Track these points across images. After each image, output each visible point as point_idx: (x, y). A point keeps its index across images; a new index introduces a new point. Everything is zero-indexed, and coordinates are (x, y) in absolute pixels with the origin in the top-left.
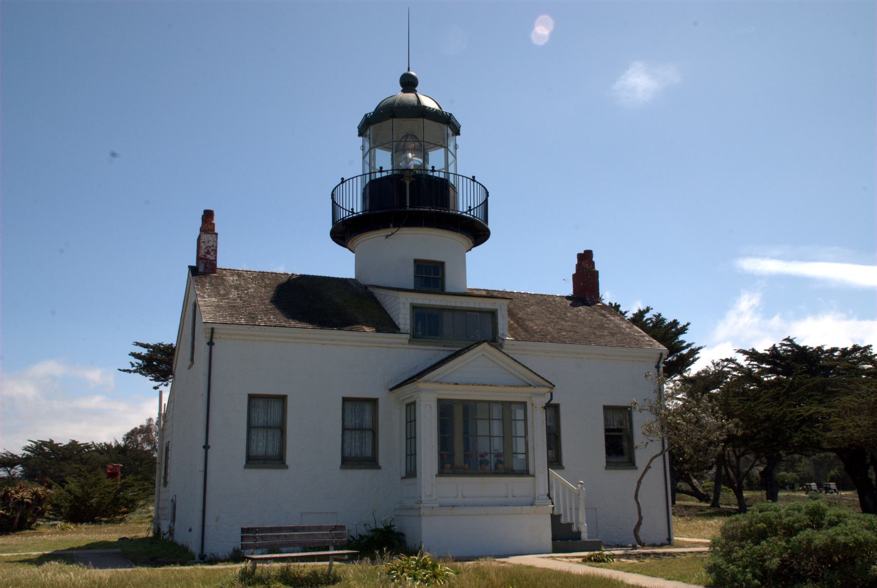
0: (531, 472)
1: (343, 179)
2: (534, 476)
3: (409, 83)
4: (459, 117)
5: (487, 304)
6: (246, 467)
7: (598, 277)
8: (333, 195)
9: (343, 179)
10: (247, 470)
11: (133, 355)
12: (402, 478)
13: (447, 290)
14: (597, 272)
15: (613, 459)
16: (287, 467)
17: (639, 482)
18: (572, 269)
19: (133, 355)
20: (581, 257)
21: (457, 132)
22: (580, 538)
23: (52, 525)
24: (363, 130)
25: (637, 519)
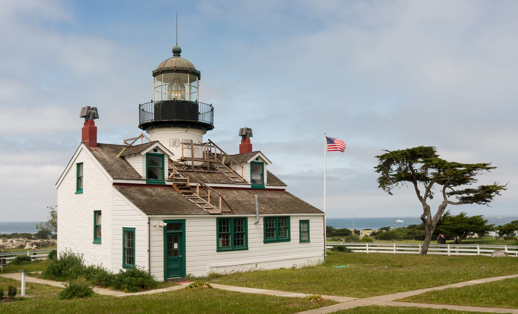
4: (197, 68)
14: (96, 127)
21: (199, 79)
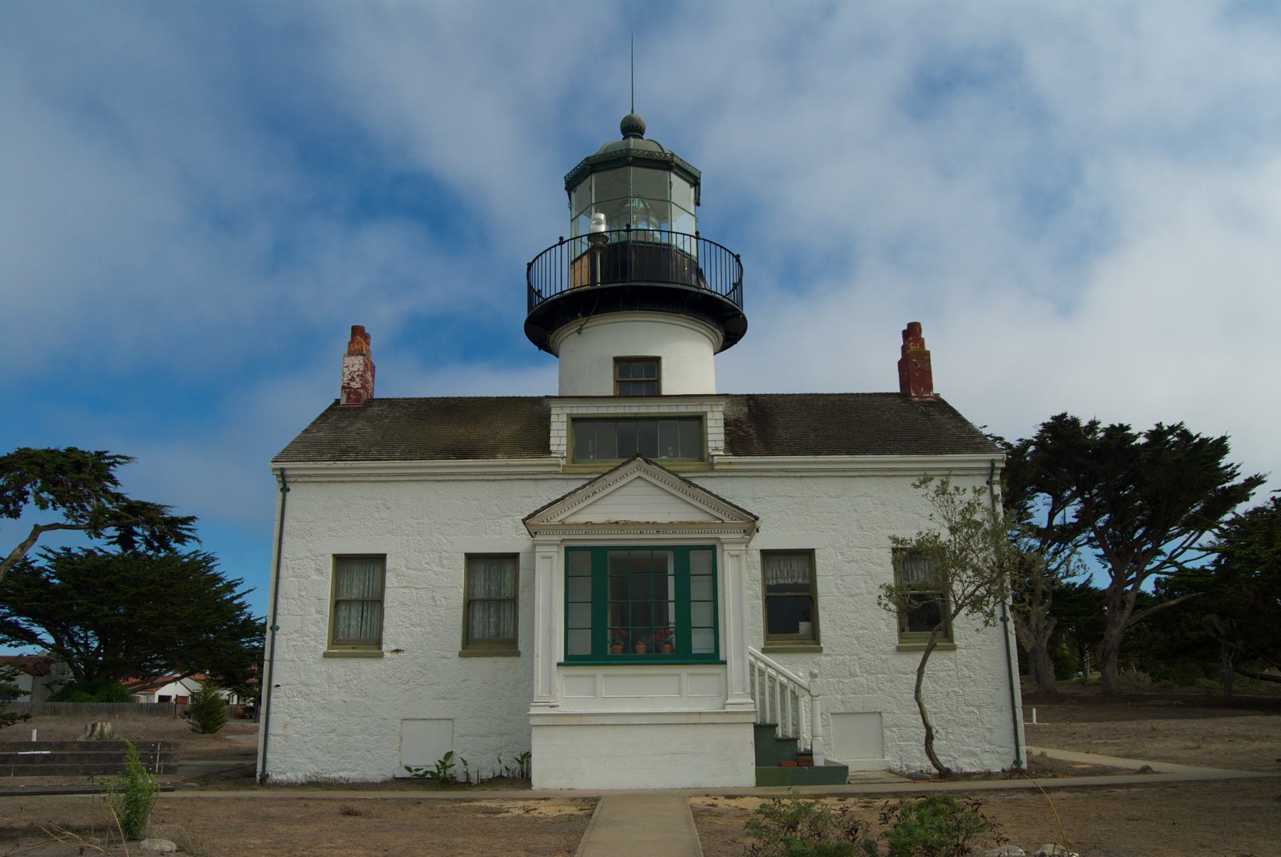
0: (722, 658)
1: (561, 238)
2: (725, 663)
3: (632, 128)
5: (692, 409)
6: (461, 655)
7: (929, 360)
8: (530, 265)
9: (561, 238)
10: (466, 661)
11: (1256, 481)
12: (559, 664)
13: (665, 391)
14: (928, 353)
15: (773, 636)
16: (518, 654)
17: (920, 672)
18: (895, 354)
19: (1256, 481)
20: (906, 334)
22: (810, 762)
23: (1010, 801)
24: (572, 183)
25: (923, 733)
